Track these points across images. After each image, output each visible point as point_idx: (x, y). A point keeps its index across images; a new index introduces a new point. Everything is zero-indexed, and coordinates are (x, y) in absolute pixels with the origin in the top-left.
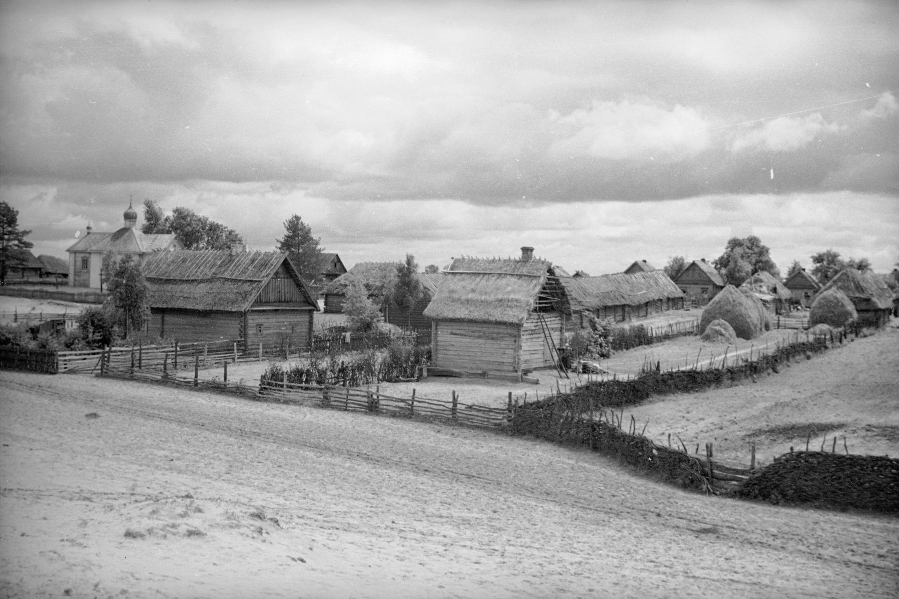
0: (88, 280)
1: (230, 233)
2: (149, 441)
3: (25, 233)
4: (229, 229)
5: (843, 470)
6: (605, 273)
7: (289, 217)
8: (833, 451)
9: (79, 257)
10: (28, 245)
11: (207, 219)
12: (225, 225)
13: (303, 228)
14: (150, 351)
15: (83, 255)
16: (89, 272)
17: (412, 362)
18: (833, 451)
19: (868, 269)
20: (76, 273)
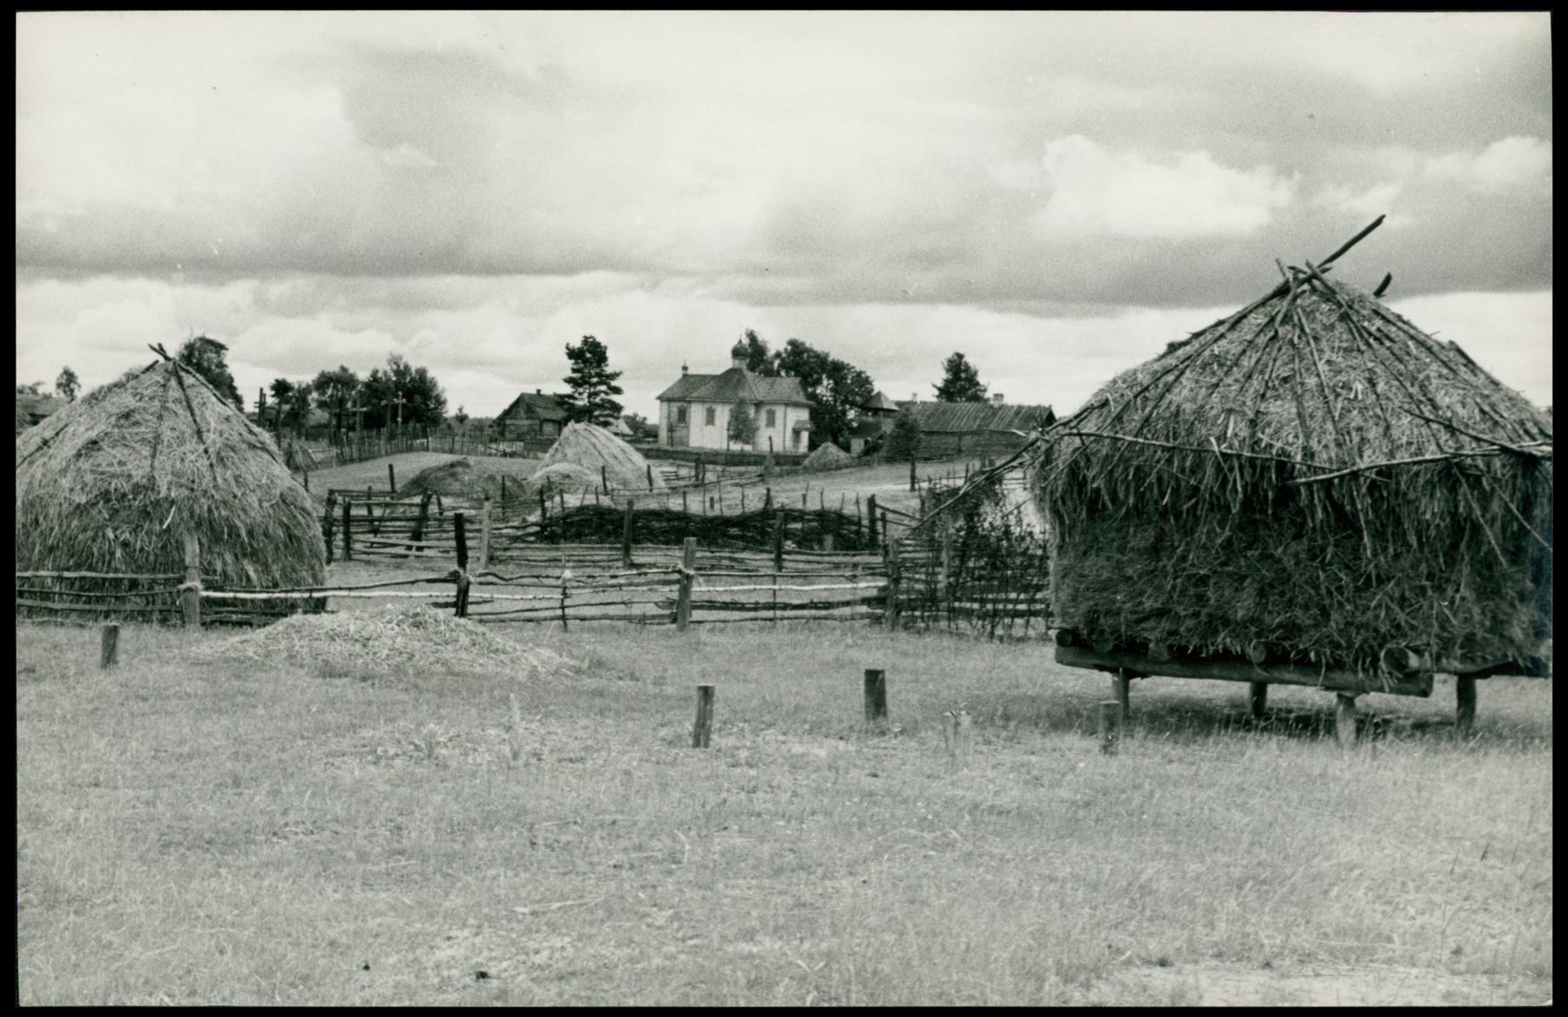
0: (688, 437)
1: (859, 374)
2: (661, 918)
3: (615, 376)
4: (858, 369)
5: (815, 872)
6: (333, 368)
7: (950, 355)
8: (472, 603)
9: (675, 407)
10: (617, 391)
11: (827, 355)
12: (852, 364)
13: (967, 368)
14: (779, 613)
15: (680, 404)
16: (687, 427)
17: (1466, 803)
18: (472, 603)
19: (939, 389)
20: (671, 429)
